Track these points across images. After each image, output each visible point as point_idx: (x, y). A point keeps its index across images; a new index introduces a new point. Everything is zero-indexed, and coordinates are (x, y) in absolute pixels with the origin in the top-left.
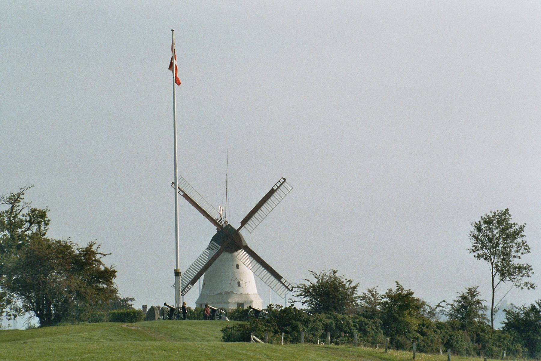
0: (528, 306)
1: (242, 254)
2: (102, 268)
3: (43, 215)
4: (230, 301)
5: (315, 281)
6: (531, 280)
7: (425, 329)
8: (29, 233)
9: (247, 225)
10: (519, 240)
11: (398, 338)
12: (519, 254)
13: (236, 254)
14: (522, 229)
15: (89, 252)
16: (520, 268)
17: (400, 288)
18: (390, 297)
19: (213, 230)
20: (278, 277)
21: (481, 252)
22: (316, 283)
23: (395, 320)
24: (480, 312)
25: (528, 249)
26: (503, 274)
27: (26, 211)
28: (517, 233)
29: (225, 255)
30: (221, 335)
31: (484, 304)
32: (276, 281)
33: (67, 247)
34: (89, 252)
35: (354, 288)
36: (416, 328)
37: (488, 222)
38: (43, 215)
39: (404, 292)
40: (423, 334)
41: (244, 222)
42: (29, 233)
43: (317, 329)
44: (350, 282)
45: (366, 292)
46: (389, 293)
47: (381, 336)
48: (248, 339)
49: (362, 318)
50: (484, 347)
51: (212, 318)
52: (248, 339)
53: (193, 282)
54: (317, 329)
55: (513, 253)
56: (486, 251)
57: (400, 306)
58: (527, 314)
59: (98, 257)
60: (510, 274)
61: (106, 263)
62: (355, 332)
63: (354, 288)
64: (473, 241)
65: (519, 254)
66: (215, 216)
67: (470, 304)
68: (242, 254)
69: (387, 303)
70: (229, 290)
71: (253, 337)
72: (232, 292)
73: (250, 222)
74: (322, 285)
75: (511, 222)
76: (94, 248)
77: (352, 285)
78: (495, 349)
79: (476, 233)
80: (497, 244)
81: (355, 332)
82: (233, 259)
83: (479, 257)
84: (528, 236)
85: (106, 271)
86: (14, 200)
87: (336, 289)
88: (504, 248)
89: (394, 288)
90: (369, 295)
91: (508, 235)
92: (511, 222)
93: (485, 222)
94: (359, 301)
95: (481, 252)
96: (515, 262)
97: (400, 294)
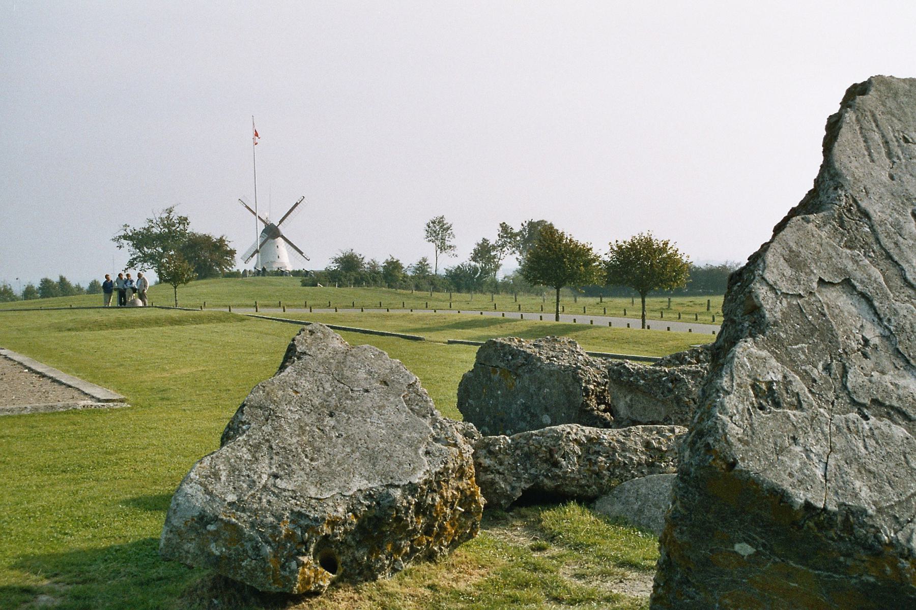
0: (456, 266)
1: (280, 239)
2: (229, 249)
3: (186, 219)
4: (274, 266)
5: (342, 255)
6: (456, 253)
7: (405, 279)
8: (178, 229)
9: (282, 223)
10: (449, 231)
11: (392, 284)
12: (450, 239)
13: (276, 239)
14: (451, 226)
15: (221, 240)
16: (450, 247)
17: (393, 258)
18: (387, 263)
19: (262, 227)
20: (301, 253)
21: (430, 238)
22: (342, 256)
23: (391, 275)
24: (429, 270)
25: (454, 236)
26: (441, 250)
27: (176, 217)
28: (448, 228)
29: (270, 241)
30: (301, 283)
31: (430, 265)
32: (300, 255)
33: (209, 238)
34: (221, 240)
35: (363, 258)
36: (401, 279)
37: (434, 222)
38: (186, 219)
39: (395, 260)
40: (405, 282)
41: (281, 222)
42: (178, 229)
43: (351, 280)
44: (360, 255)
45: (370, 260)
46: (387, 262)
47: (384, 283)
48: (316, 285)
49: (373, 274)
50: (435, 287)
51: (282, 275)
52: (316, 285)
53: (252, 256)
54: (351, 280)
55: (447, 239)
56: (433, 238)
57: (393, 267)
58: (456, 270)
59: (226, 243)
60: (445, 249)
61: (231, 246)
62: (371, 281)
63: (363, 258)
64: (426, 232)
65: (450, 239)
66: (264, 219)
67: (424, 265)
68: (280, 239)
69: (385, 266)
70: (273, 260)
71: (318, 284)
72: (274, 262)
73: (284, 221)
74: (345, 257)
75: (445, 222)
76: (224, 238)
77: (362, 257)
78: (441, 288)
79: (427, 228)
80: (438, 234)
81: (371, 281)
82: (275, 243)
83: (429, 241)
84: (454, 229)
85: (231, 250)
86: (170, 211)
87: (353, 259)
88: (442, 236)
89: (389, 259)
90: (372, 262)
91: (444, 230)
92: (445, 222)
93: (432, 223)
94: (366, 266)
95: (430, 238)
96: (448, 243)
97: (392, 262)
